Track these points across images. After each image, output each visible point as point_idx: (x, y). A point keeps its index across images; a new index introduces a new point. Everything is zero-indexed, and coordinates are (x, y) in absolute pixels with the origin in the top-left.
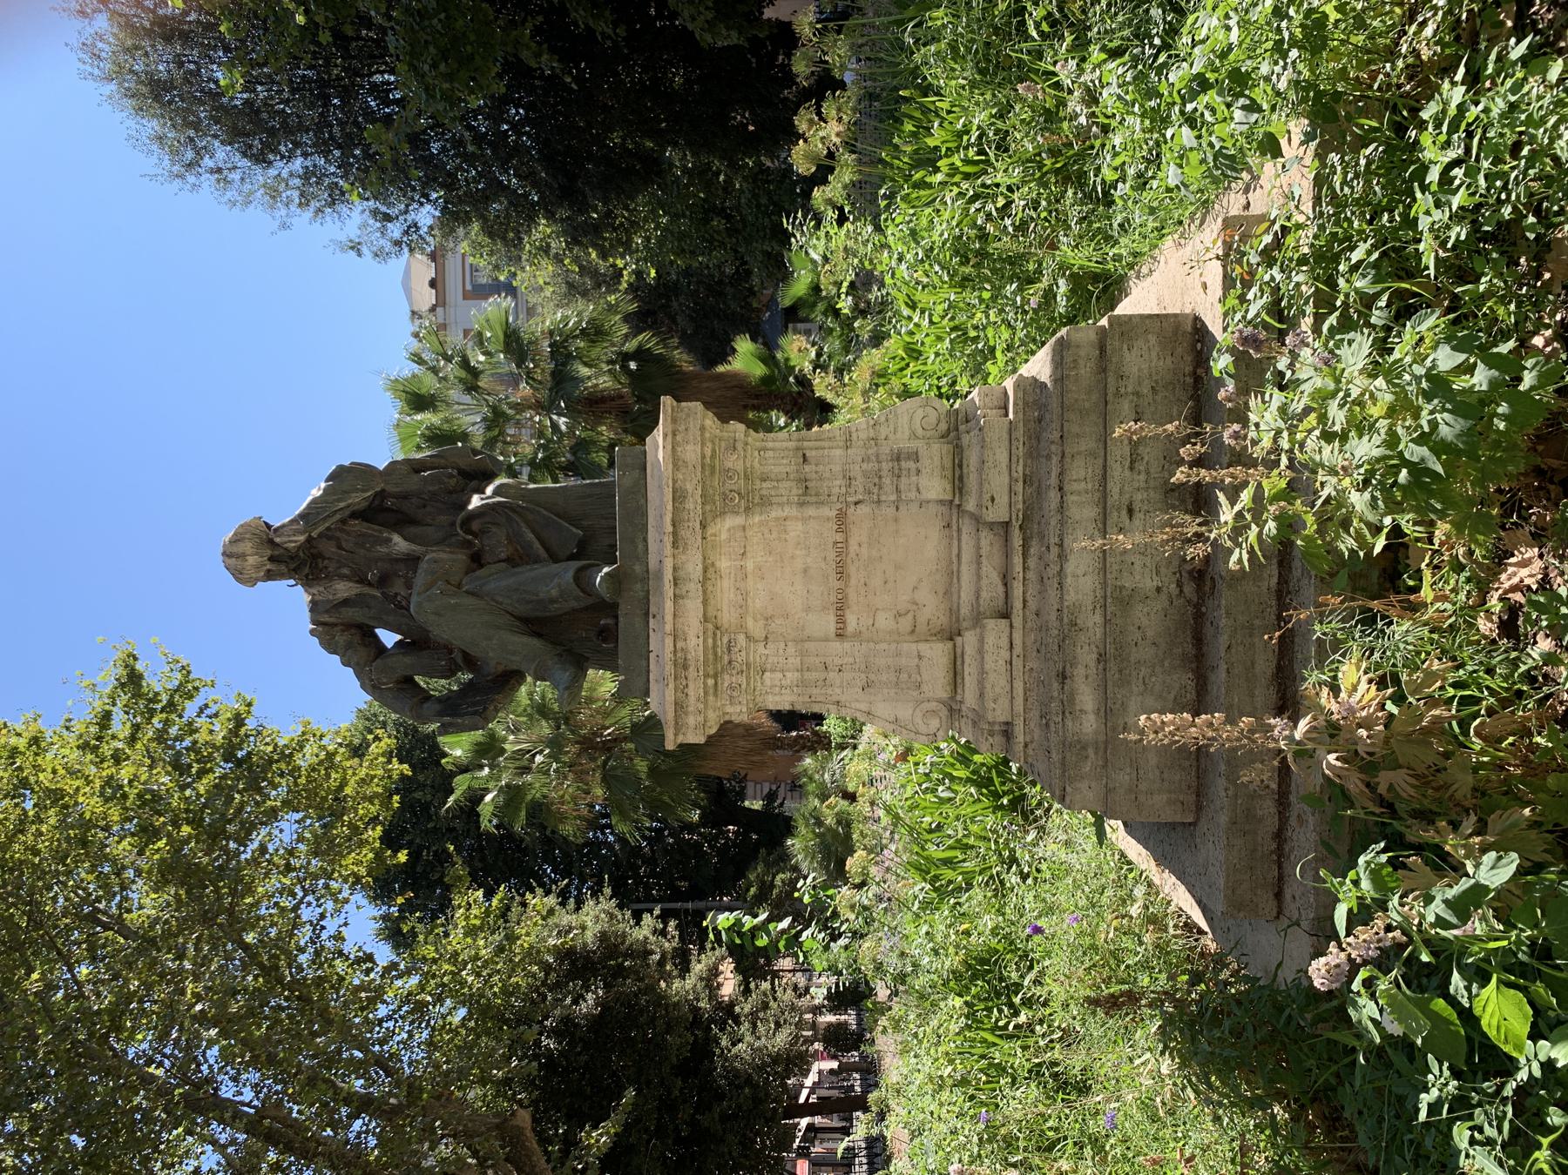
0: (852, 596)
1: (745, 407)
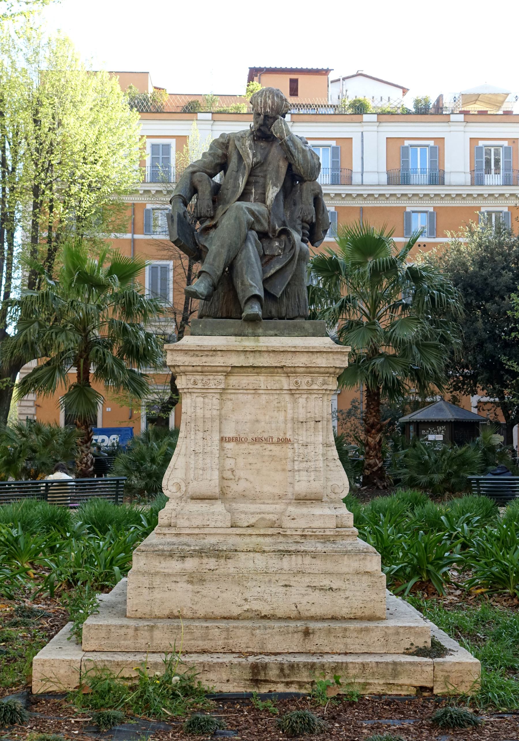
0: (244, 446)
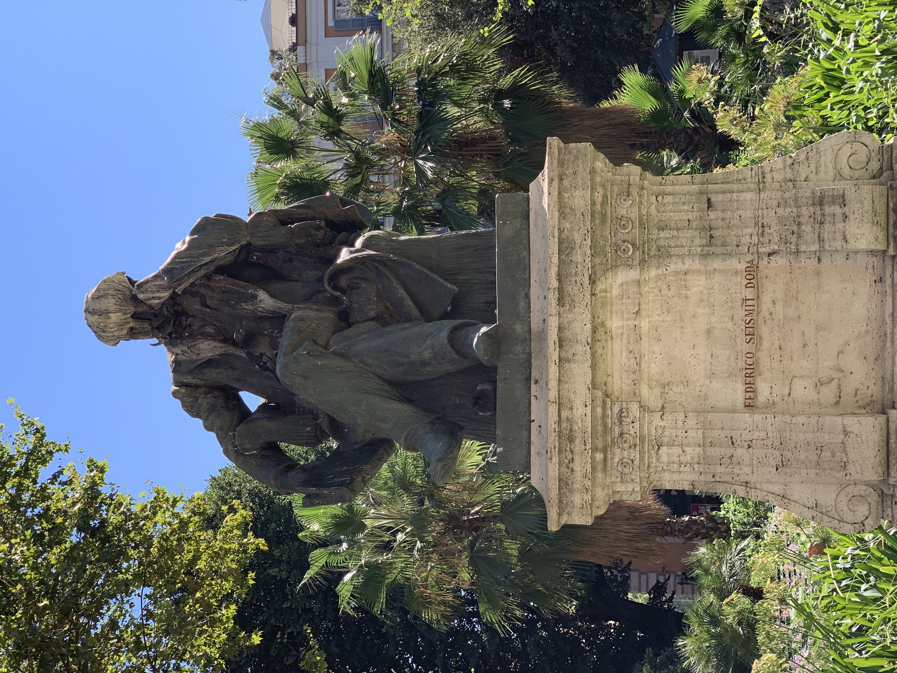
1: (633, 146)
